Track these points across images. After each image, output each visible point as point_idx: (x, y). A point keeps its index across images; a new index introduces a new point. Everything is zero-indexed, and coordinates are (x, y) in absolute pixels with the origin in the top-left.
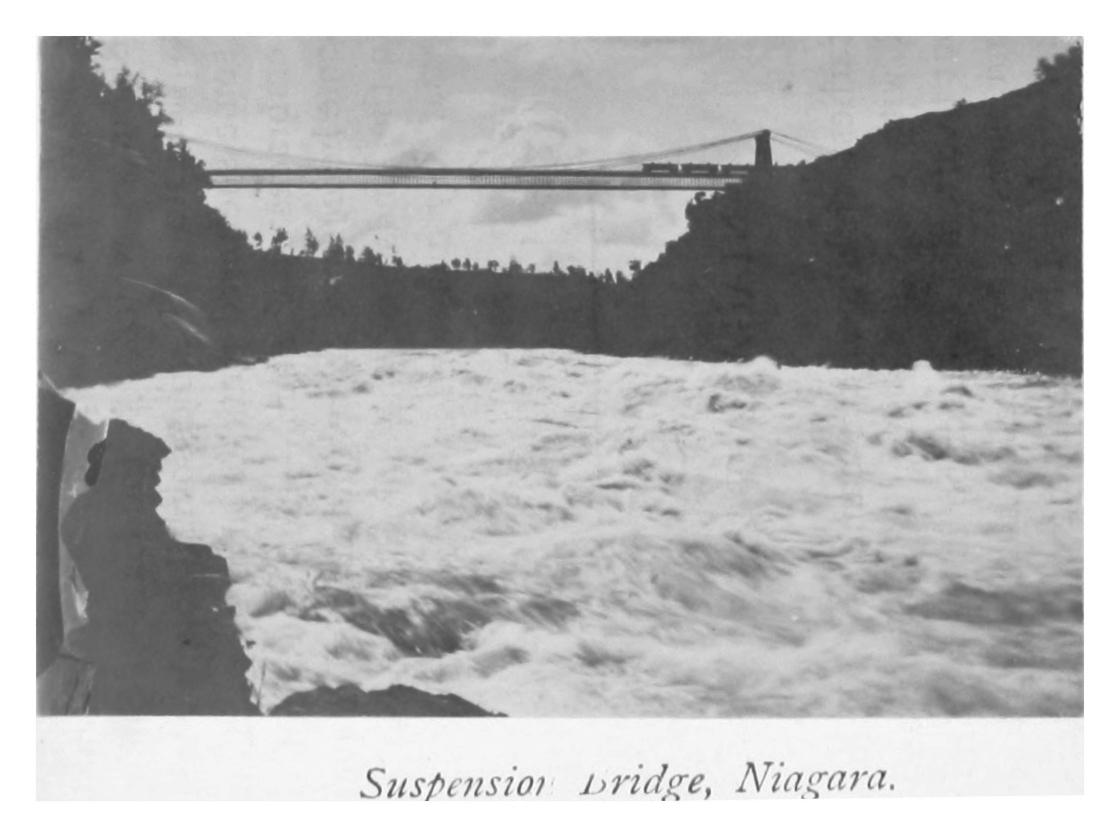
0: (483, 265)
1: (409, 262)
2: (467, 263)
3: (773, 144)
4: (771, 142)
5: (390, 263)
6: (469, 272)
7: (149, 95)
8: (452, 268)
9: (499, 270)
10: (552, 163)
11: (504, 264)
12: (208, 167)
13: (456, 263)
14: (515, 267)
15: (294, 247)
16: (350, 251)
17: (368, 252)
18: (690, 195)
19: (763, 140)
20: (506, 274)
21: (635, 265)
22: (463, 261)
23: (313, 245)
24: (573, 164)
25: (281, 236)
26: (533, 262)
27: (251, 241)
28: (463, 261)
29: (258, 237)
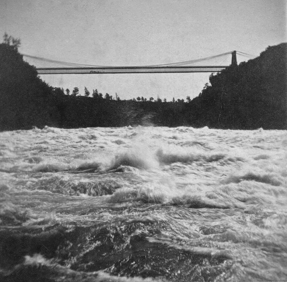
0: (148, 99)
1: (122, 99)
2: (143, 98)
3: (237, 55)
4: (237, 54)
5: (115, 99)
6: (143, 102)
7: (15, 44)
8: (137, 101)
9: (153, 101)
10: (190, 59)
11: (155, 99)
12: (37, 67)
13: (139, 99)
14: (159, 100)
15: (82, 93)
16: (101, 95)
17: (107, 95)
18: (210, 73)
19: (234, 54)
20: (155, 103)
21: (188, 98)
22: (141, 98)
23: (87, 93)
24: (196, 61)
25: (76, 90)
26: (112, 95)
27: (65, 93)
28: (141, 98)
29: (68, 90)
